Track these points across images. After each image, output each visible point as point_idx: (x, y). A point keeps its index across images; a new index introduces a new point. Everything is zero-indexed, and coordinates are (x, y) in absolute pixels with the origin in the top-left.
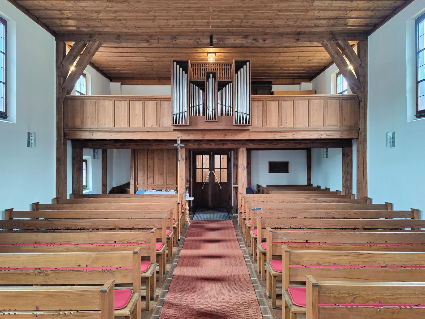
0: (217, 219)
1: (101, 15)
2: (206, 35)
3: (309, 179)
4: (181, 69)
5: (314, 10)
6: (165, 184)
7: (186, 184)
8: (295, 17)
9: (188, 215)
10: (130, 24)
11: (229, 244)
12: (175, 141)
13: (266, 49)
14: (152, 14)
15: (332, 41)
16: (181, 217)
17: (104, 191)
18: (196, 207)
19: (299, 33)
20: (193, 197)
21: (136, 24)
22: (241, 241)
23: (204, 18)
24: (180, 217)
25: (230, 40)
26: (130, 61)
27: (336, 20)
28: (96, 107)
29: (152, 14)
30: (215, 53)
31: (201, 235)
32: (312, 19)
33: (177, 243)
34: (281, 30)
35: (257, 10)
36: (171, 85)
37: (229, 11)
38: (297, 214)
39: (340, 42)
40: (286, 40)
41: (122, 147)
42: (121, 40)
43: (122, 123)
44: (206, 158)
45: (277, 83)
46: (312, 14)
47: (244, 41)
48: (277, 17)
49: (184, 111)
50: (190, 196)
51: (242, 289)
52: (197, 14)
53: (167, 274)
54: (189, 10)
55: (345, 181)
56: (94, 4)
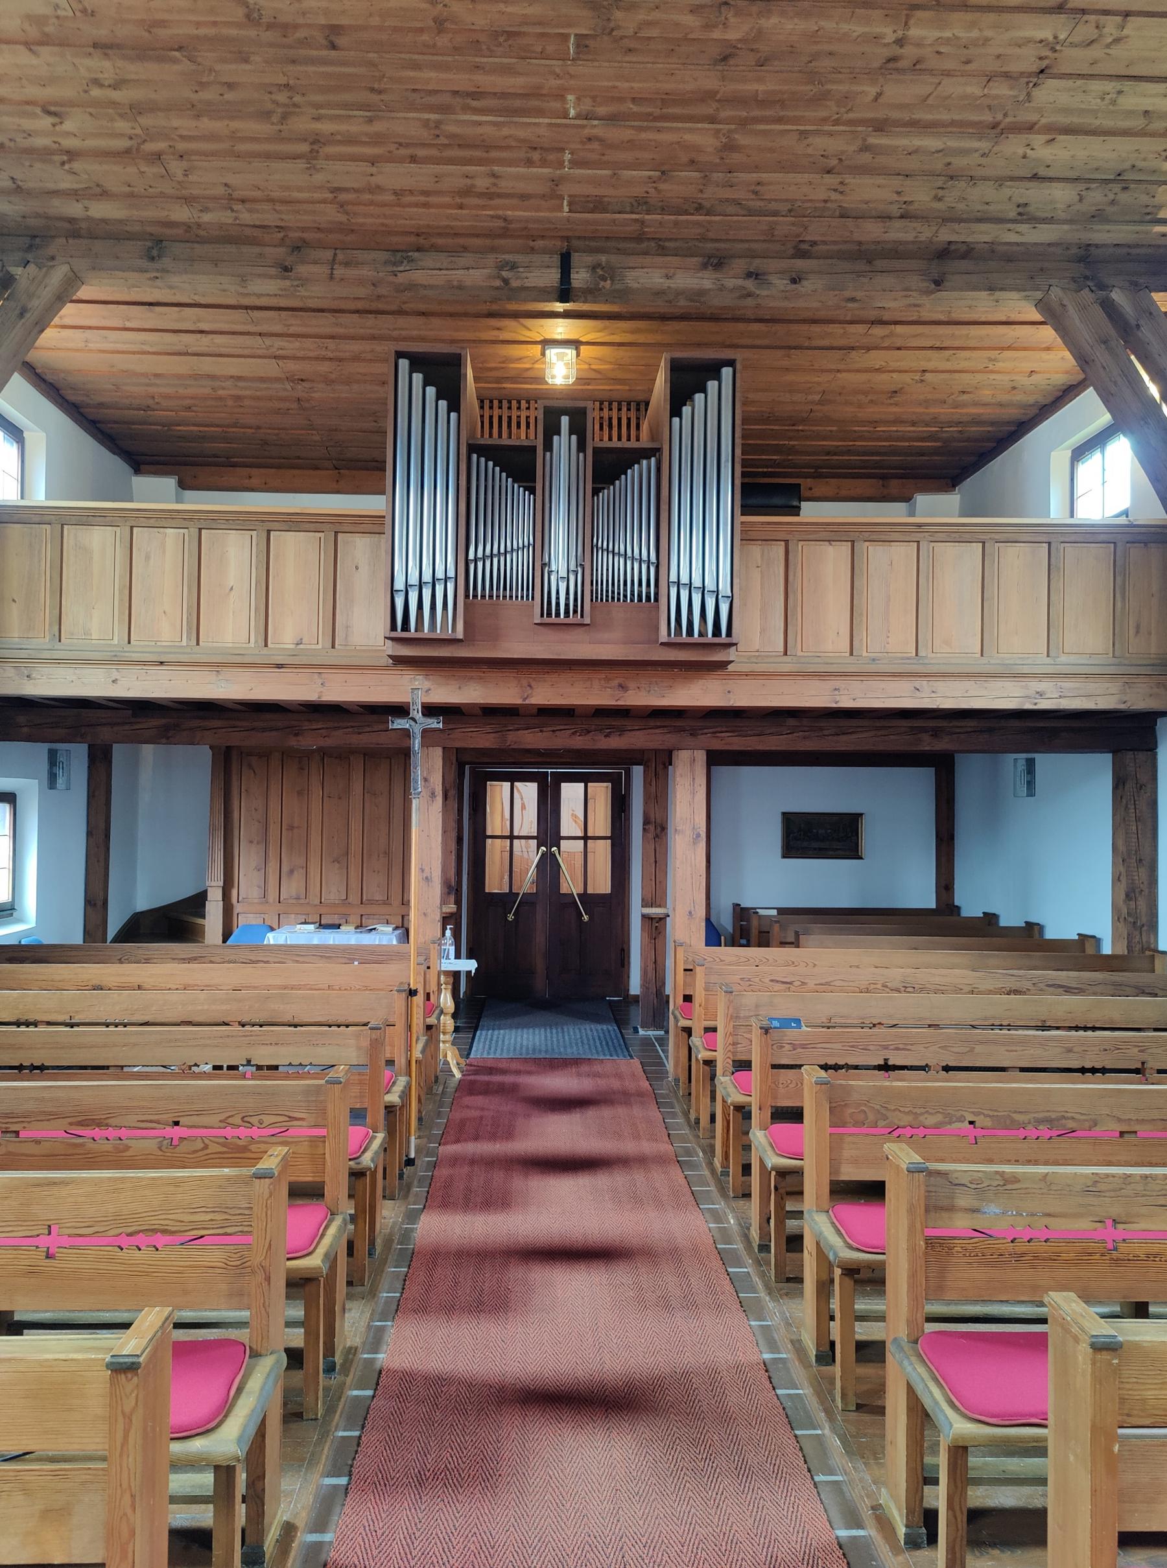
0: (571, 1052)
1: (68, 126)
2: (544, 251)
3: (945, 884)
4: (431, 391)
5: (1030, 128)
6: (354, 898)
7: (444, 902)
8: (939, 166)
9: (449, 1038)
10: (209, 178)
11: (639, 1177)
12: (401, 710)
13: (795, 327)
14: (302, 124)
15: (1086, 292)
16: (423, 1052)
17: (94, 929)
18: (479, 1003)
19: (945, 253)
20: (470, 956)
21: (231, 179)
22: (692, 1166)
23: (536, 156)
24: (417, 1053)
25: (648, 277)
26: (212, 377)
27: (1117, 188)
28: (48, 553)
29: (302, 124)
30: (575, 344)
31: (509, 1135)
32: (1012, 179)
33: (401, 1176)
34: (871, 231)
35: (780, 120)
36: (383, 493)
37: (656, 119)
38: (972, 1050)
39: (1117, 296)
40: (889, 280)
41: (164, 736)
42: (166, 262)
43: (162, 625)
44: (528, 791)
45: (817, 492)
46: (1020, 151)
47: (706, 281)
48: (866, 158)
49: (440, 574)
50: (458, 956)
51: (743, 1472)
52: (506, 131)
53: (346, 1369)
54: (477, 111)
55: (1128, 896)
56: (34, 61)
